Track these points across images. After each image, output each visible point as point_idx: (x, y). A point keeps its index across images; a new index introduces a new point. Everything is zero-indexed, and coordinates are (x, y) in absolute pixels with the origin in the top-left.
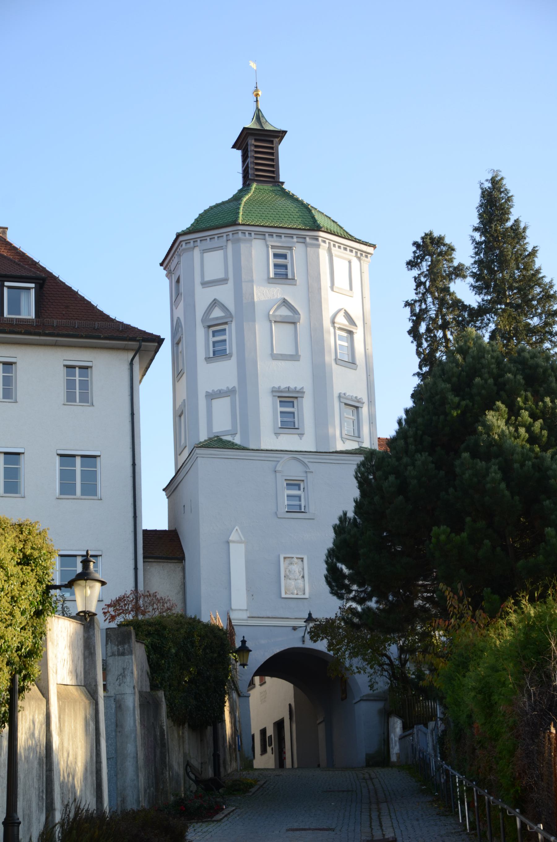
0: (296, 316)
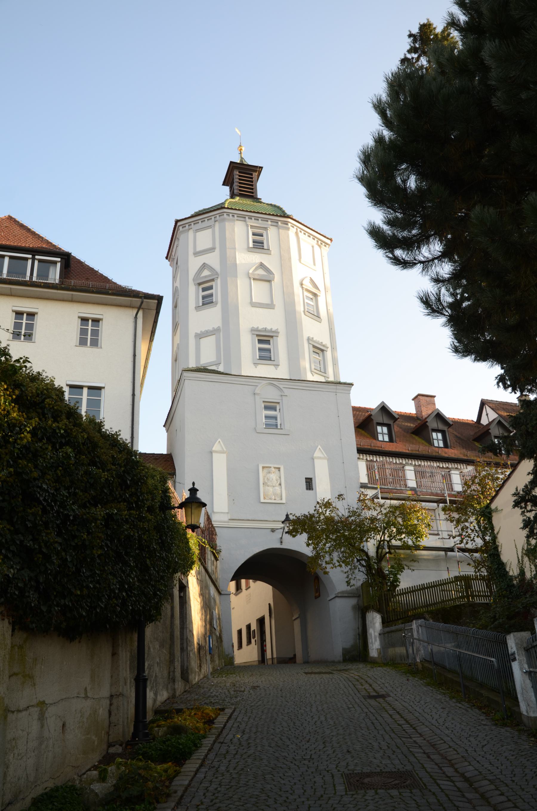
0: (271, 276)
